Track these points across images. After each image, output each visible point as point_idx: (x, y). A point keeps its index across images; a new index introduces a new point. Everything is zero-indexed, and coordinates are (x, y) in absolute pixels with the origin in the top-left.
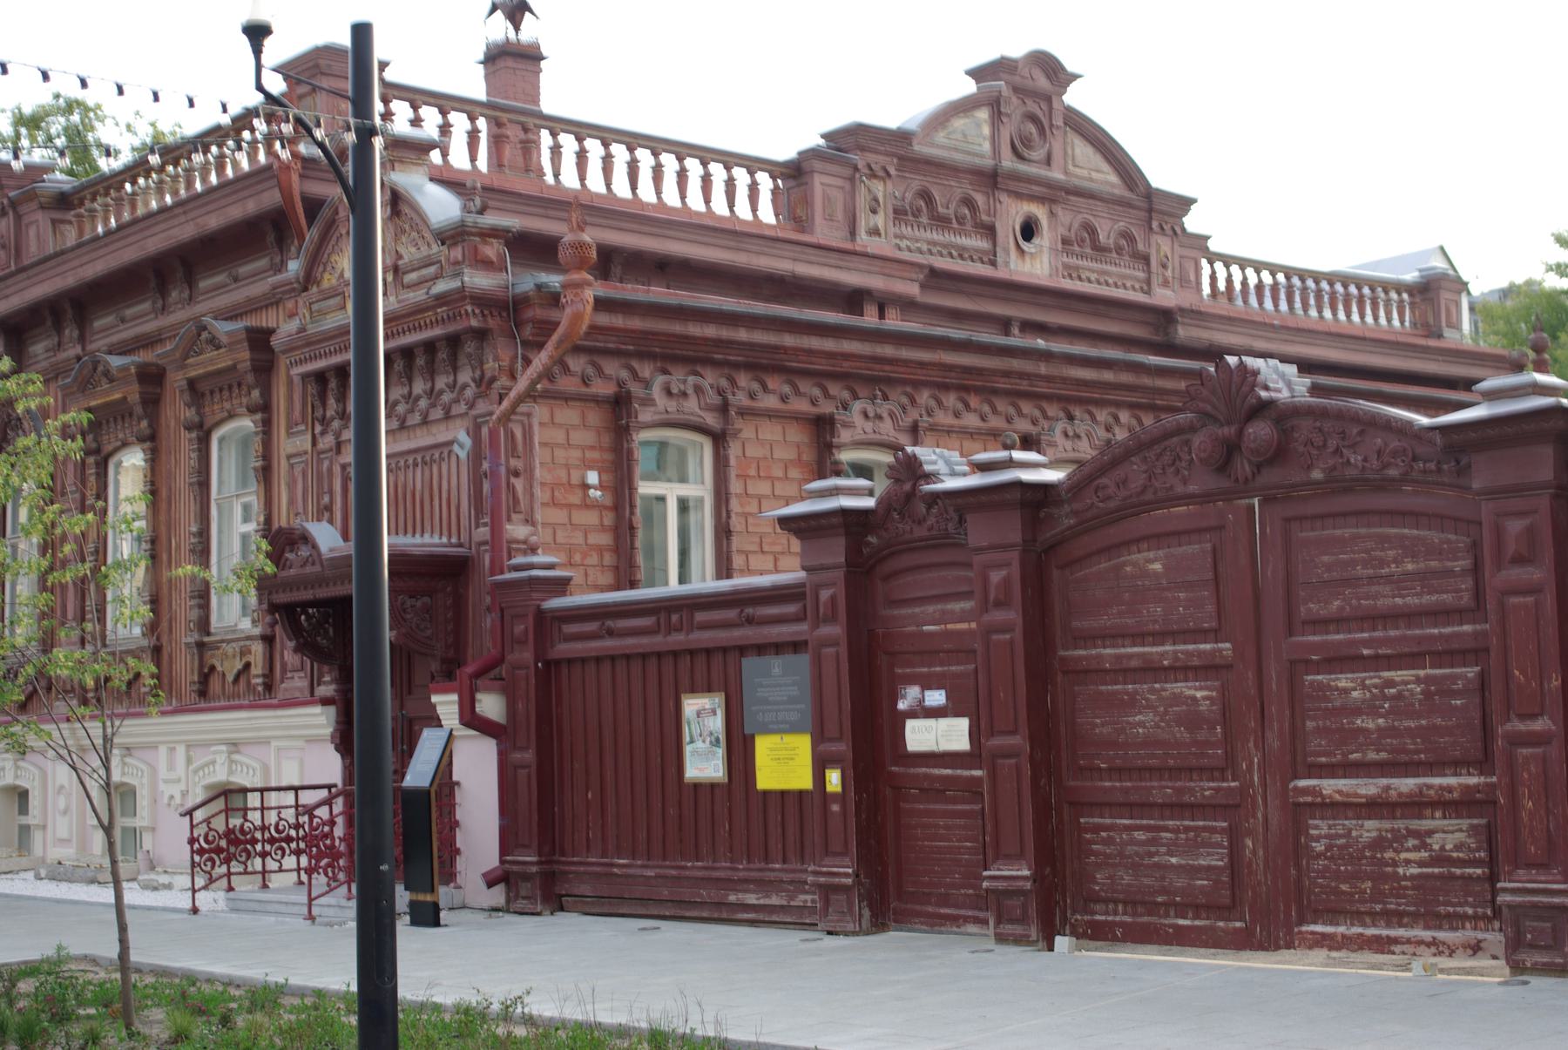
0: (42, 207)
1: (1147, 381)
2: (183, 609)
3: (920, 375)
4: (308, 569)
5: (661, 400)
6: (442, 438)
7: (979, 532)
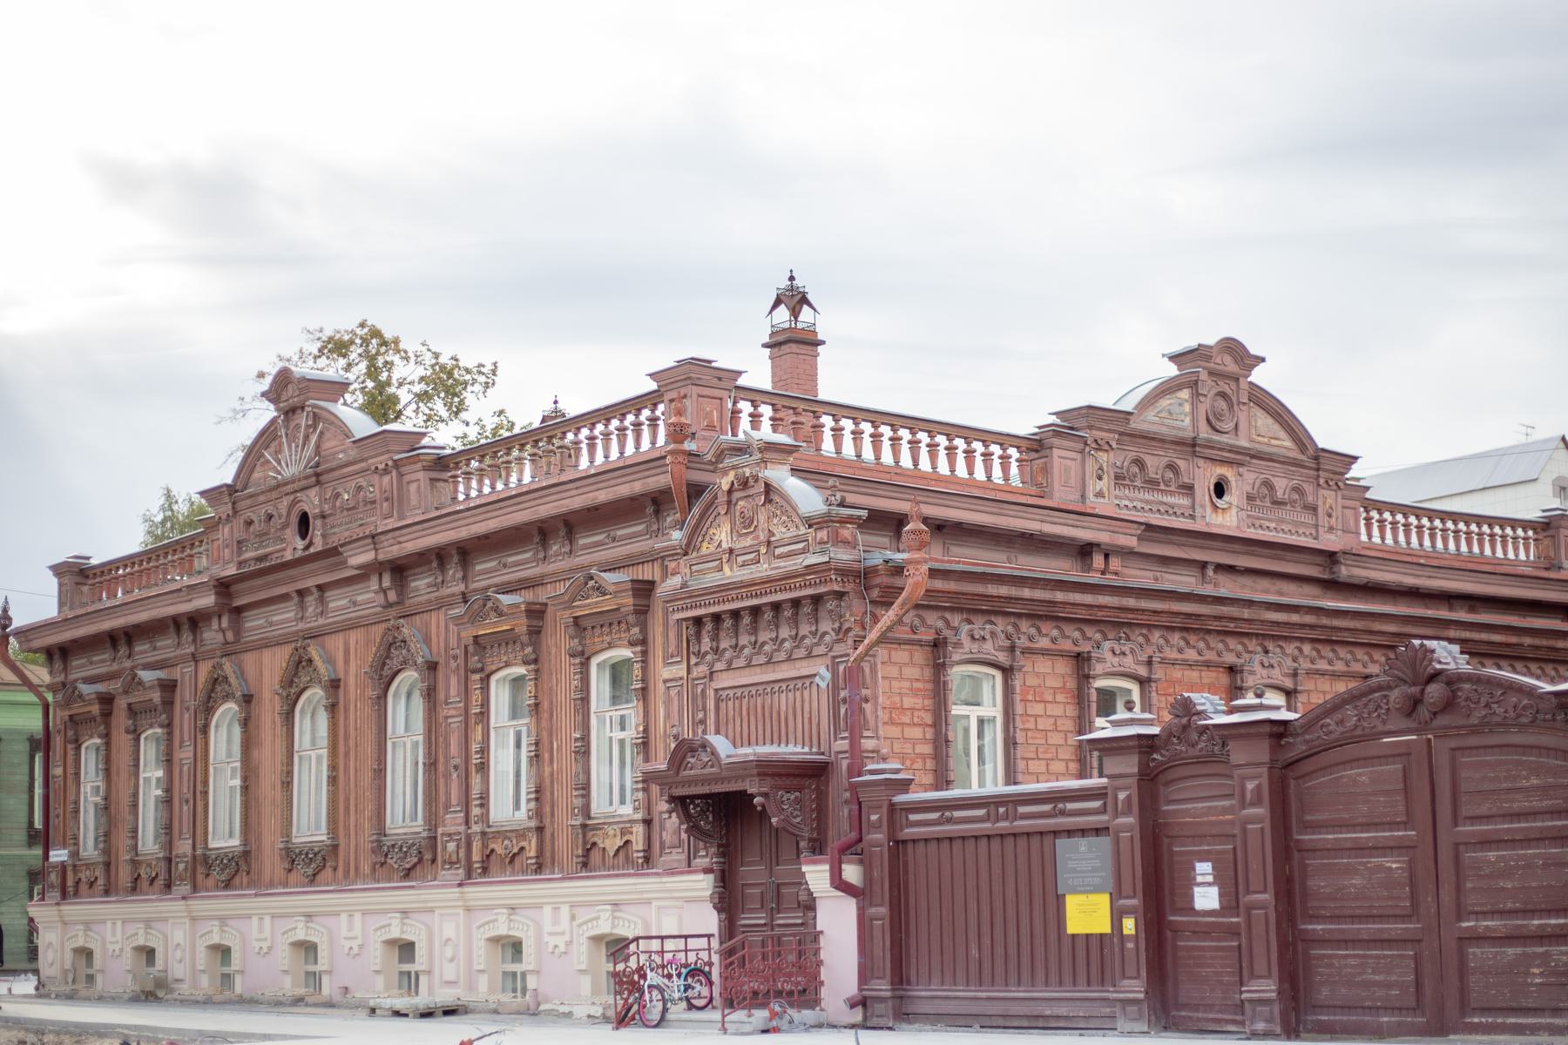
0: (425, 469)
1: (1325, 621)
2: (564, 797)
3: (1154, 620)
4: (708, 770)
5: (967, 644)
6: (805, 672)
7: (1239, 754)
